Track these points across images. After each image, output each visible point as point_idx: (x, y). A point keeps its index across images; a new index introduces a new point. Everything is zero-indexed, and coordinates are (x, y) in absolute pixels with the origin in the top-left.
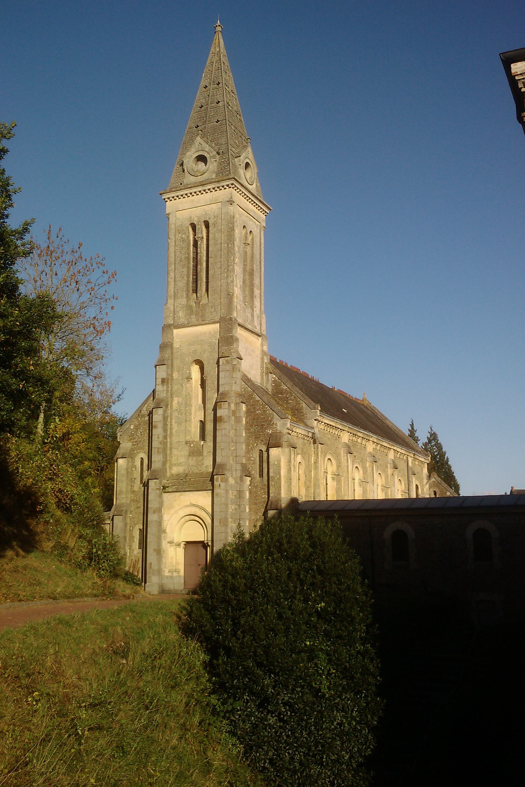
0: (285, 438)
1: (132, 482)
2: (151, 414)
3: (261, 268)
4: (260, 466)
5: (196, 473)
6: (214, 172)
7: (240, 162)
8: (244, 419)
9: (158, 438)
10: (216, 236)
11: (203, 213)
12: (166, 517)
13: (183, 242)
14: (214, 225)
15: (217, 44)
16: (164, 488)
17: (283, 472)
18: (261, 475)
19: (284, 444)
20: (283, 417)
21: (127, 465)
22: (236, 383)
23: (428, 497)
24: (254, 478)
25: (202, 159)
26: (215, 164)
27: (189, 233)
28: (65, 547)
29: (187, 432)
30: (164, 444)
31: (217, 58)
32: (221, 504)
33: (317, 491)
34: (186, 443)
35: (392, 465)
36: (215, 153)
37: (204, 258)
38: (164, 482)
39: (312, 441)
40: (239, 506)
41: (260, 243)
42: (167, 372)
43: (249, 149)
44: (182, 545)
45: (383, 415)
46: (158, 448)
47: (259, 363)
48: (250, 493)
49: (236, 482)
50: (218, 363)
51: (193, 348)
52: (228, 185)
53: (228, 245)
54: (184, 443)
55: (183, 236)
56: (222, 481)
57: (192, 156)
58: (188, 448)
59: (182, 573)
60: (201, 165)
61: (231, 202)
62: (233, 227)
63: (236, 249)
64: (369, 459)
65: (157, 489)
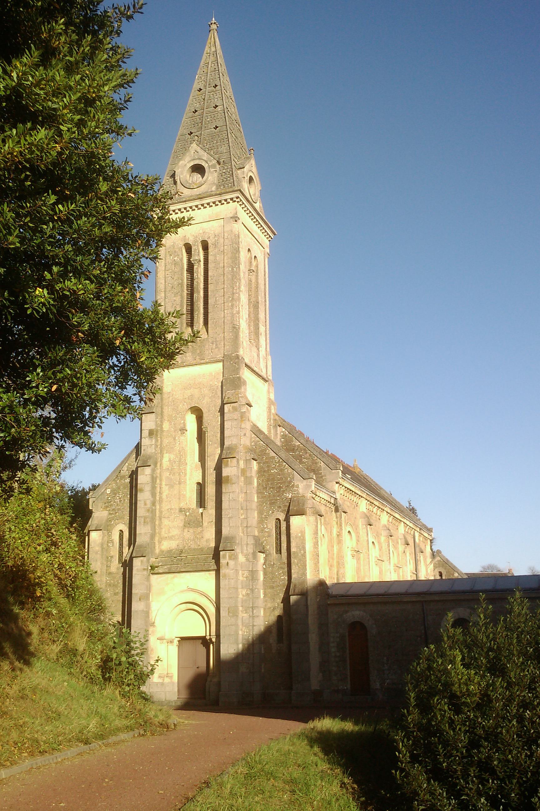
0: (309, 504)
1: (107, 561)
2: (134, 475)
3: (265, 301)
4: (277, 539)
5: (194, 549)
6: (214, 184)
7: (243, 174)
8: (255, 480)
9: (145, 504)
10: (218, 258)
11: (201, 232)
12: (154, 606)
13: (175, 266)
14: (215, 245)
15: (212, 43)
16: (153, 568)
17: (309, 546)
18: (279, 551)
19: (308, 511)
20: (307, 477)
21: (103, 539)
22: (245, 435)
23: (432, 578)
24: (270, 554)
25: (198, 169)
26: (216, 175)
27: (182, 255)
28: (74, 652)
29: (181, 496)
30: (152, 511)
31: (212, 58)
32: (229, 588)
33: (341, 571)
34: (181, 510)
35: (403, 540)
36: (215, 162)
37: (202, 285)
38: (153, 560)
39: (333, 508)
40: (252, 590)
41: (265, 271)
42: (156, 422)
43: (253, 162)
44: (176, 642)
45: (377, 484)
46: (145, 518)
47: (265, 415)
48: (265, 574)
49: (247, 560)
50: (222, 411)
51: (188, 392)
52: (232, 199)
53: (232, 269)
54: (177, 511)
55: (176, 258)
56: (230, 558)
57: (185, 165)
58: (182, 517)
59: (175, 679)
60: (197, 177)
61: (236, 219)
62: (239, 248)
63: (242, 274)
64: (384, 533)
65: (144, 569)
